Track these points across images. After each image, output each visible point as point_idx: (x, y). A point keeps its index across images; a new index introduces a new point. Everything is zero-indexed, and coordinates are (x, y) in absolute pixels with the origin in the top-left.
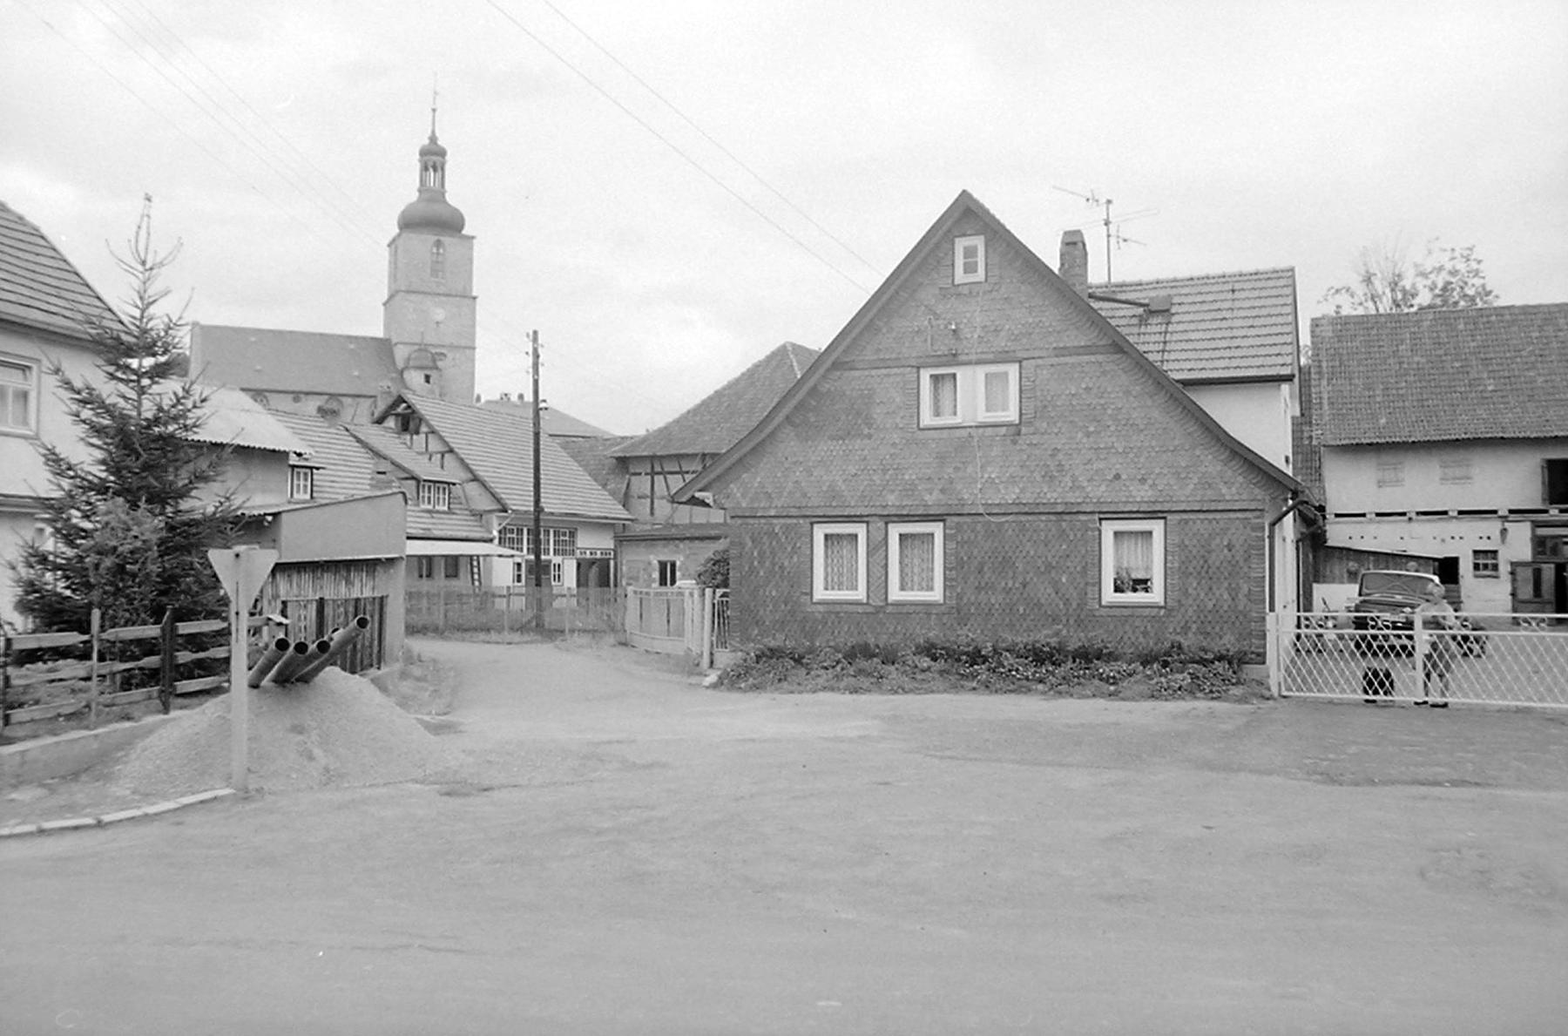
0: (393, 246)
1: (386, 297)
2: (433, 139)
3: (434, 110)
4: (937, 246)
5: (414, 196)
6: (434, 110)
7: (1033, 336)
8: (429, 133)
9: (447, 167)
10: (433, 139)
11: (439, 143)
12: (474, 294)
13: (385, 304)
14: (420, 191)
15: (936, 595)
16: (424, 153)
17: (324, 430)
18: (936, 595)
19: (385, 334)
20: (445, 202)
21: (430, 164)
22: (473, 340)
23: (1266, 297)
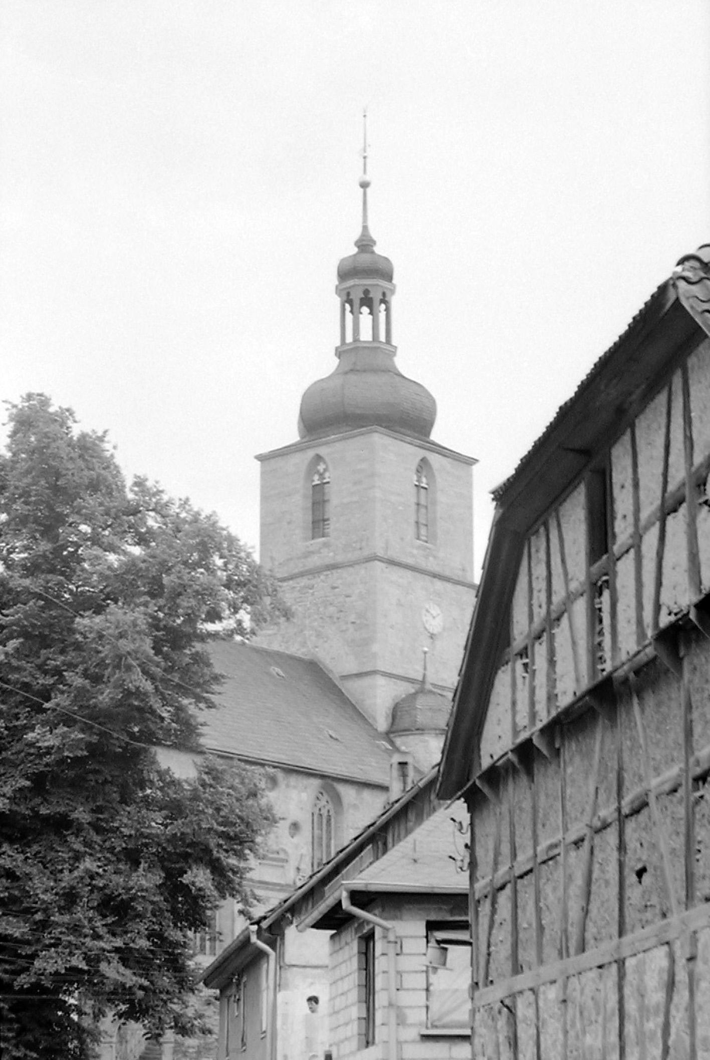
2: (365, 244)
3: (364, 185)
6: (364, 185)
8: (357, 234)
9: (395, 301)
10: (365, 244)
11: (378, 250)
16: (347, 273)
21: (357, 295)
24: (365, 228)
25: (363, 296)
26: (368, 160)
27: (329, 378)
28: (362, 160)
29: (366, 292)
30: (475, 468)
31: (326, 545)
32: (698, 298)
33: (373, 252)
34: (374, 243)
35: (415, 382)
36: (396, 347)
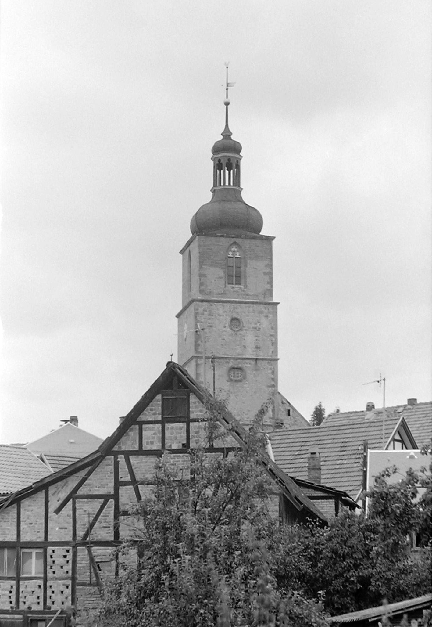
0: (187, 252)
1: (180, 308)
2: (227, 134)
3: (227, 104)
4: (96, 459)
5: (208, 197)
6: (227, 104)
7: (247, 441)
8: (222, 129)
9: (243, 164)
10: (227, 134)
11: (233, 137)
12: (275, 300)
13: (178, 316)
14: (213, 191)
15: (113, 457)
16: (216, 150)
17: (369, 438)
18: (113, 457)
19: (41, 558)
20: (241, 201)
21: (224, 162)
22: (275, 352)
23: (332, 431)
24: (227, 125)
25: (227, 161)
26: (228, 90)
27: (212, 198)
28: (226, 91)
29: (229, 160)
30: (278, 306)
31: (233, 607)
32: (365, 464)
33: (231, 139)
34: (231, 134)
35: (252, 207)
36: (242, 157)
